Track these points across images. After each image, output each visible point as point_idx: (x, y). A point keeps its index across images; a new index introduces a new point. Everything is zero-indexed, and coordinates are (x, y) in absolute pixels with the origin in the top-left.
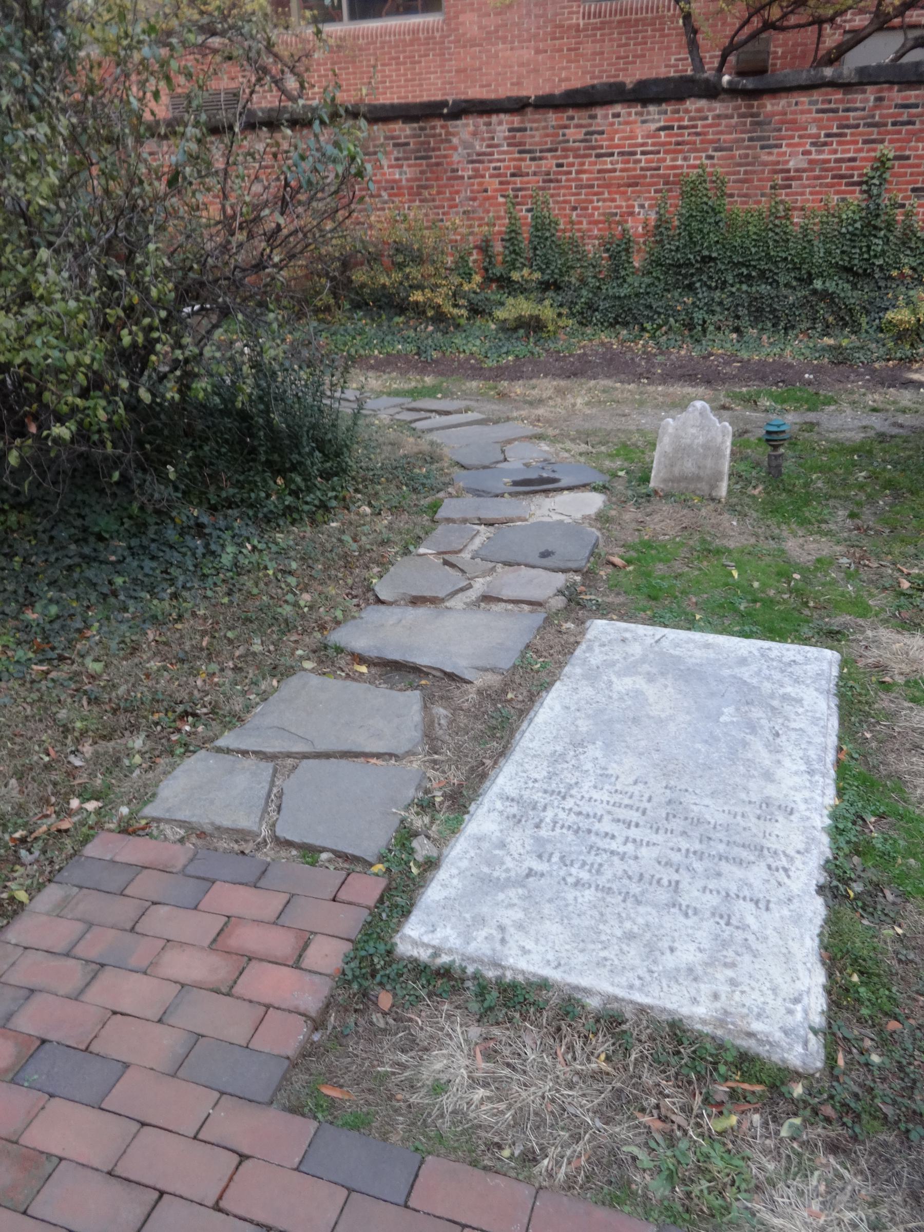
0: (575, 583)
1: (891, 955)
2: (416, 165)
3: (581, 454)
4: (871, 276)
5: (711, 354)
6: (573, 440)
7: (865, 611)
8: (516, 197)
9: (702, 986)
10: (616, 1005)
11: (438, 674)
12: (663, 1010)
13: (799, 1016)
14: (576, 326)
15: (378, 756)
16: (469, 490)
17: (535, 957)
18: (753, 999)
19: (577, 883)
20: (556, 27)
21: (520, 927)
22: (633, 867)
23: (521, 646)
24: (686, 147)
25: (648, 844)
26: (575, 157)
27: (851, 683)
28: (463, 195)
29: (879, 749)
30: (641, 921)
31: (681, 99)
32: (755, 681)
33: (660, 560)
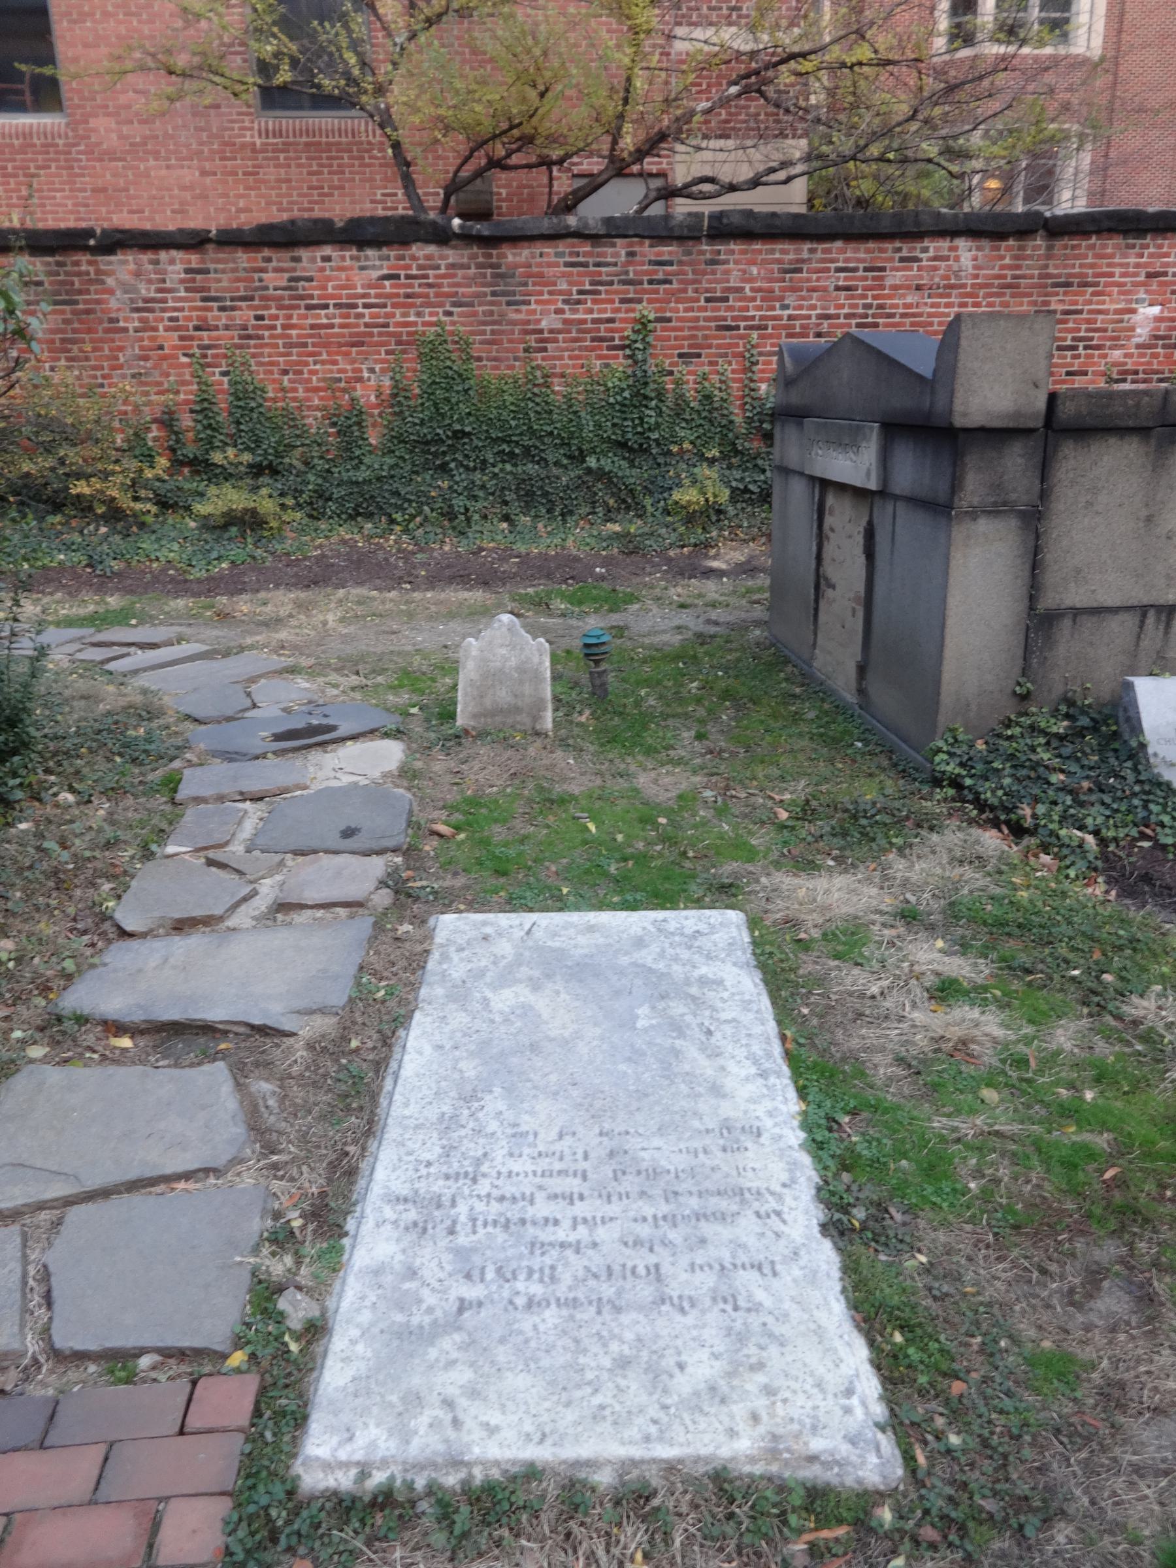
0: (397, 869)
1: (923, 1293)
3: (353, 689)
4: (647, 451)
5: (481, 549)
6: (337, 670)
7: (751, 855)
8: (205, 356)
9: (734, 1408)
10: (635, 1473)
11: (241, 1030)
12: (697, 1460)
13: (859, 1412)
14: (306, 520)
15: (187, 1176)
16: (215, 754)
17: (508, 1434)
18: (800, 1406)
19: (531, 1304)
21: (474, 1393)
22: (595, 1260)
23: (353, 970)
24: (419, 301)
25: (603, 1222)
26: (279, 308)
27: (768, 949)
28: (129, 352)
29: (821, 1026)
30: (629, 1336)
31: (405, 243)
32: (661, 966)
33: (496, 821)
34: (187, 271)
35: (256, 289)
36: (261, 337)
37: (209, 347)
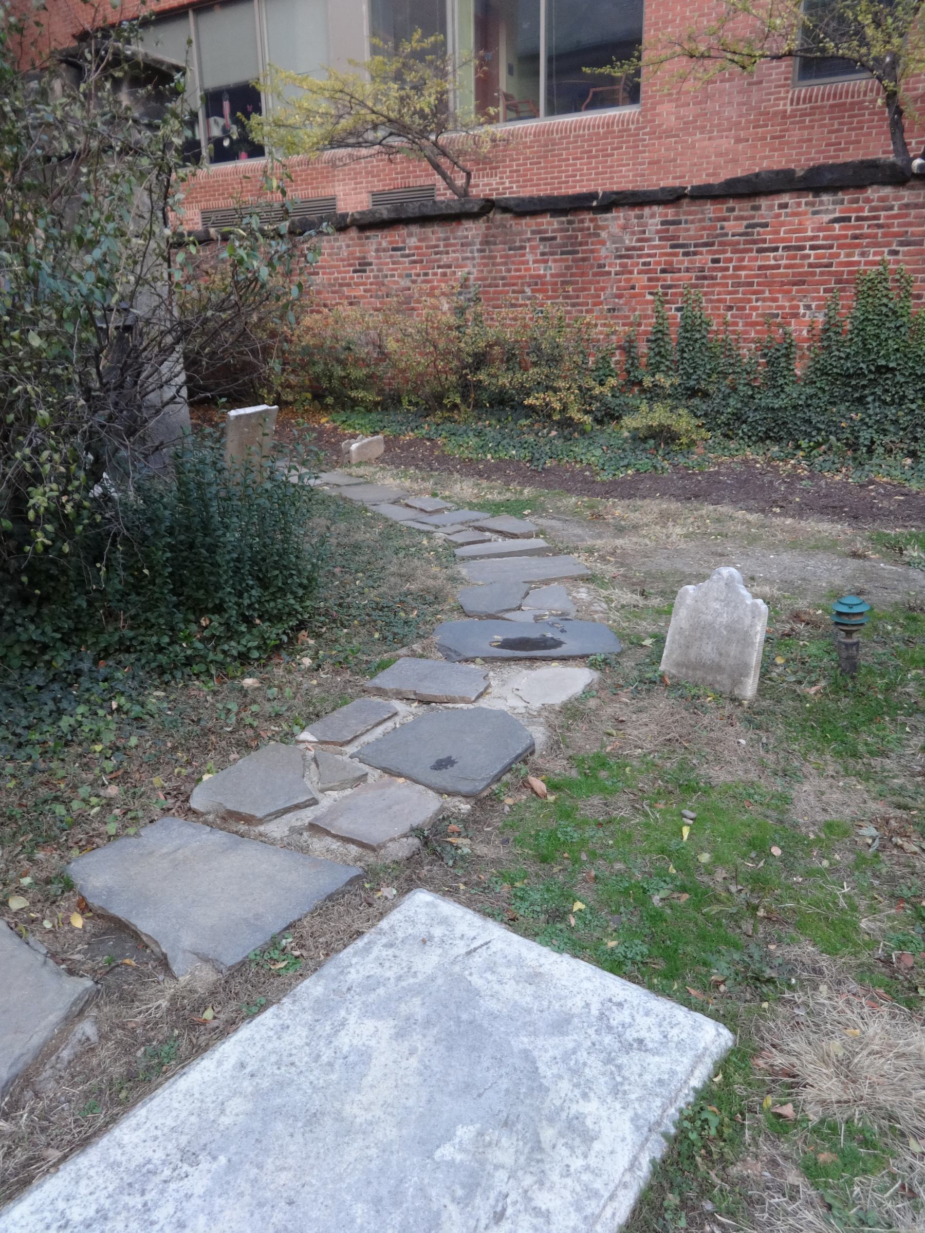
2: (561, 260)
8: (666, 294)
20: (761, 114)
28: (608, 292)
34: (663, 223)
35: (717, 236)
36: (713, 278)
37: (670, 287)
